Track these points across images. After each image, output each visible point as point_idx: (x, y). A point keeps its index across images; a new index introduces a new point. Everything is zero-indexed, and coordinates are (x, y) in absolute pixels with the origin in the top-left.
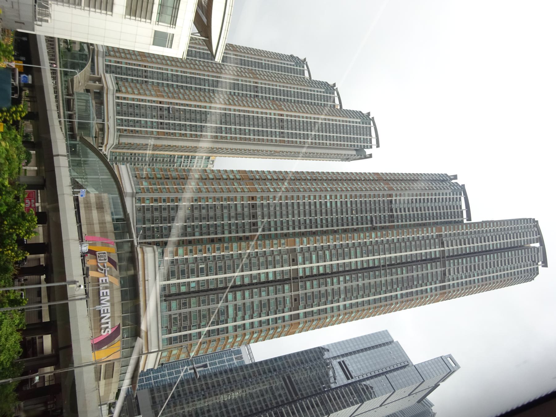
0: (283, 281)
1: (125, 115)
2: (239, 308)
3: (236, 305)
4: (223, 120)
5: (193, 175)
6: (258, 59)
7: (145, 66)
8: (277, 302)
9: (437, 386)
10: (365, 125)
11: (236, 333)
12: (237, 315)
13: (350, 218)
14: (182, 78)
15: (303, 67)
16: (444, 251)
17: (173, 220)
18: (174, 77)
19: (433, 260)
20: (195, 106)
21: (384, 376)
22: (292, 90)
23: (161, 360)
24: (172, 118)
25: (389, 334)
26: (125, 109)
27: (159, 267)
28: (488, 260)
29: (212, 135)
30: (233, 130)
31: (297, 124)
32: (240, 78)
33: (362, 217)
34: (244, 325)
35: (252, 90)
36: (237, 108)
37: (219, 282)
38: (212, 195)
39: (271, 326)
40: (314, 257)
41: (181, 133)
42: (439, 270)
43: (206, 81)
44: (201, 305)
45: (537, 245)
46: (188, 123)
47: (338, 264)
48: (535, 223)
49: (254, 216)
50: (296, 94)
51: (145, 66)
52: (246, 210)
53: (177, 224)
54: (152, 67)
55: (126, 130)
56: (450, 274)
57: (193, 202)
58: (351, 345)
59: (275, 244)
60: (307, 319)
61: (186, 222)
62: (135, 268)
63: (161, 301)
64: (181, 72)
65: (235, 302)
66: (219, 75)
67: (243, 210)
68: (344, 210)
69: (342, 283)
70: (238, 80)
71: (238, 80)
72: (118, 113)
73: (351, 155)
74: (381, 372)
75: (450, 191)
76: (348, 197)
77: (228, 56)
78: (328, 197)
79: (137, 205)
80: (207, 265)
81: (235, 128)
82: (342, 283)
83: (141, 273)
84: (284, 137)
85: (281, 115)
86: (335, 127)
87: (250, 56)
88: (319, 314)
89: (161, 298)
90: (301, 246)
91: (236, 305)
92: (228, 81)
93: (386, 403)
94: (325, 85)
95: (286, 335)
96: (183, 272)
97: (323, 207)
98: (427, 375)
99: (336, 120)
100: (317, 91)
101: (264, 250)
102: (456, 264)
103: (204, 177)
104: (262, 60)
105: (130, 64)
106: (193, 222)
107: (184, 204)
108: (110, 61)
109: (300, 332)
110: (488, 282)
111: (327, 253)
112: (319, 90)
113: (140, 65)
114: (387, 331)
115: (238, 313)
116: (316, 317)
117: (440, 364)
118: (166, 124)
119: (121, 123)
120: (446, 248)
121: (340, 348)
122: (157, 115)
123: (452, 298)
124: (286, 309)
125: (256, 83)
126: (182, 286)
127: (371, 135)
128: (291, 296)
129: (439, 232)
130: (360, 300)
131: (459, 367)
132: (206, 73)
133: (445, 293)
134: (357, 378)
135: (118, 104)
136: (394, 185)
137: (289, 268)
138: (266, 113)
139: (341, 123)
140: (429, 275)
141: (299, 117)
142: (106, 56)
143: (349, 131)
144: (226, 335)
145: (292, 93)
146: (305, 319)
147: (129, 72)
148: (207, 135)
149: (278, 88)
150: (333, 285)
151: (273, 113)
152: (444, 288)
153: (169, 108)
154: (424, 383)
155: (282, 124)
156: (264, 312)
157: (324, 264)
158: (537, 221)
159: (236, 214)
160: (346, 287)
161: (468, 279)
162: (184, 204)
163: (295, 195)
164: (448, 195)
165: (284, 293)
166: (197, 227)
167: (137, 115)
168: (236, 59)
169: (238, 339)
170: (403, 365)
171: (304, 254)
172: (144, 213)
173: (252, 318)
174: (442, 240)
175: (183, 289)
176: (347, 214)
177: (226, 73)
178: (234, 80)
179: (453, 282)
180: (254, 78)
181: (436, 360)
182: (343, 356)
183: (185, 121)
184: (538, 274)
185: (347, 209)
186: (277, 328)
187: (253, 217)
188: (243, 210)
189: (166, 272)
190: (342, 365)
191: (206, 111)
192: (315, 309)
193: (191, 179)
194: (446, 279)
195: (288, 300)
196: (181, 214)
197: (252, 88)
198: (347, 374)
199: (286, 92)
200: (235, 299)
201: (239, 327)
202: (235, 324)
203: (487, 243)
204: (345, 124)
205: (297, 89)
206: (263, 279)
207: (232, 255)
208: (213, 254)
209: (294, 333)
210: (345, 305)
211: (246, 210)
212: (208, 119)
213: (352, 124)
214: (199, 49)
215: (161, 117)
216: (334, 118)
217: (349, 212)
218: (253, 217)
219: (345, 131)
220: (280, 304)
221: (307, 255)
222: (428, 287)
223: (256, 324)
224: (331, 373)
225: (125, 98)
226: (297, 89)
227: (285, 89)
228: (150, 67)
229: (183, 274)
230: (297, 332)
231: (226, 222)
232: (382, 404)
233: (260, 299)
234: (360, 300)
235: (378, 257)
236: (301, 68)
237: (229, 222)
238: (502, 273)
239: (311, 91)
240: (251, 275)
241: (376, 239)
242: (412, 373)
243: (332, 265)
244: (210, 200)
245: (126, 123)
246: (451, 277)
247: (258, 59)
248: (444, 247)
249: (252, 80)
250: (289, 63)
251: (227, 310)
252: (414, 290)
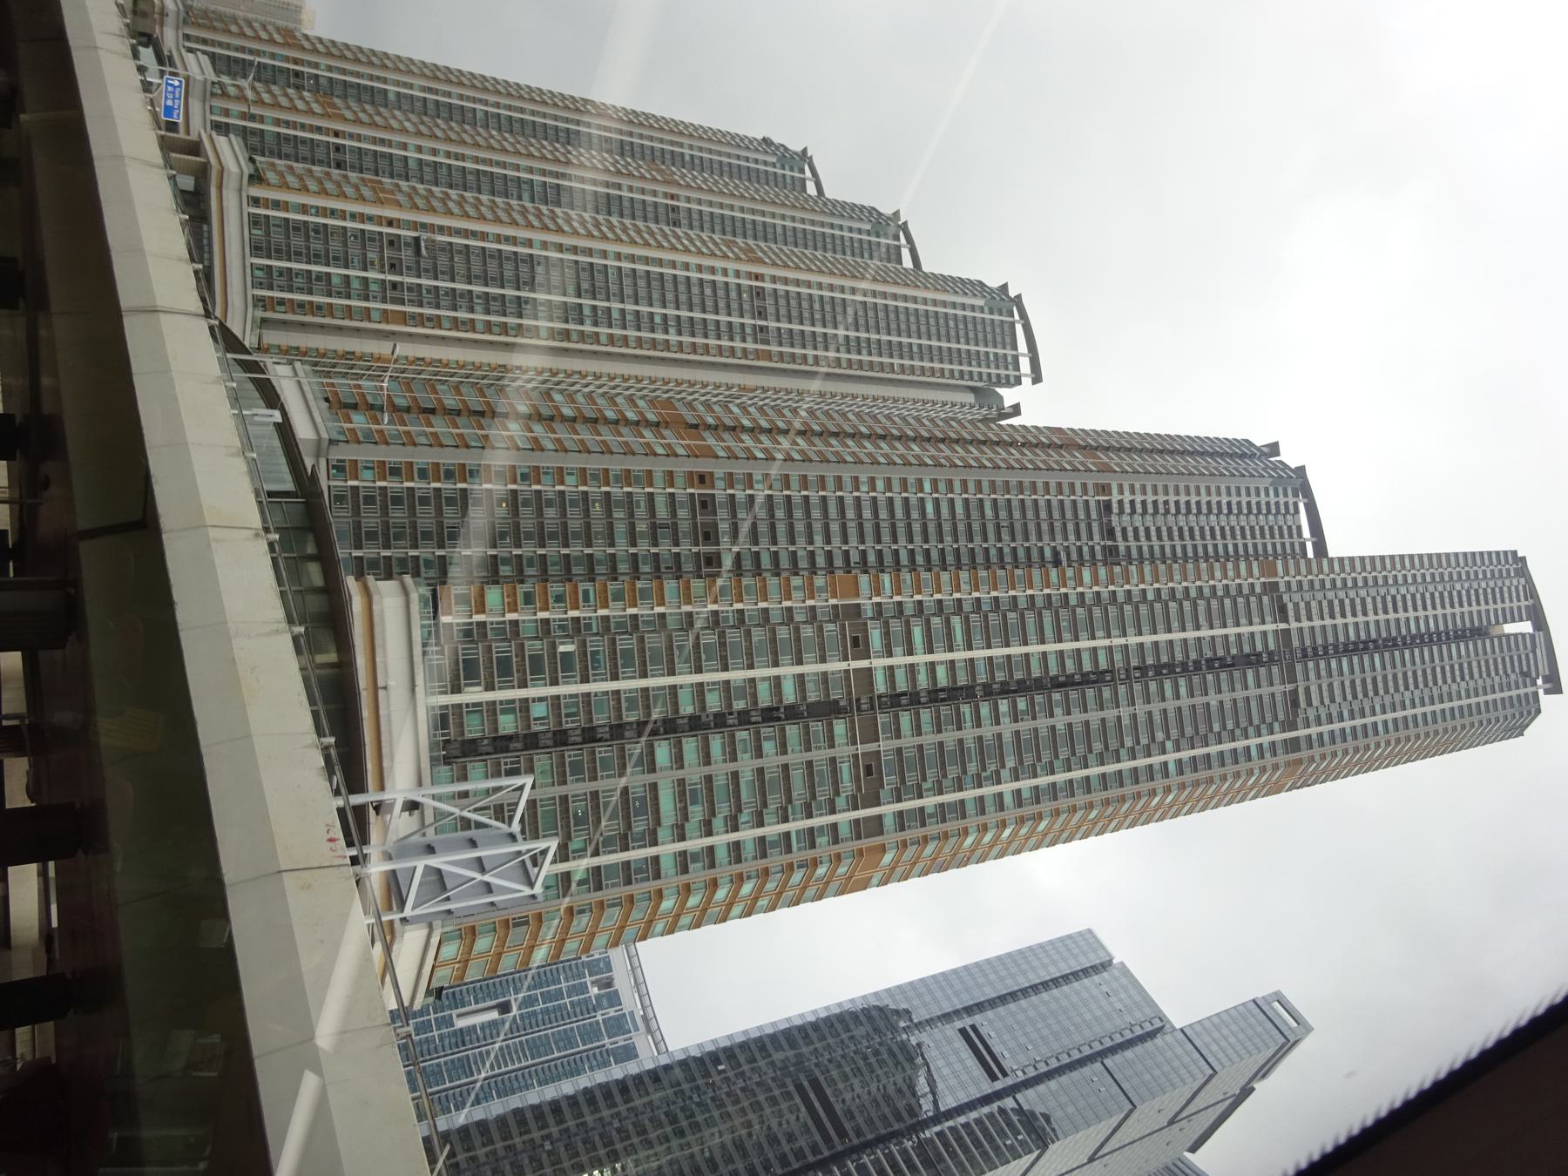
0: (829, 710)
1: (280, 254)
2: (694, 792)
3: (681, 782)
4: (585, 286)
5: (511, 405)
6: (672, 143)
7: (336, 134)
8: (811, 774)
9: (1247, 1091)
10: (996, 317)
11: (684, 878)
12: (686, 818)
13: (993, 552)
14: (450, 174)
15: (802, 171)
16: (1287, 633)
17: (454, 536)
18: (426, 169)
19: (1252, 660)
20: (498, 239)
21: (1098, 1065)
22: (778, 222)
23: (439, 973)
24: (426, 270)
25: (1098, 941)
26: (277, 237)
27: (424, 645)
28: (1408, 664)
29: (552, 329)
30: (615, 315)
31: (805, 304)
32: (625, 182)
33: (1028, 549)
34: (711, 849)
35: (662, 217)
36: (626, 250)
37: (624, 705)
38: (573, 462)
39: (797, 855)
40: (917, 633)
41: (456, 319)
42: (1278, 689)
43: (524, 186)
44: (569, 778)
45: (1526, 627)
46: (477, 289)
47: (990, 658)
48: (1515, 564)
49: (710, 535)
50: (789, 233)
51: (336, 134)
52: (683, 513)
53: (466, 552)
54: (359, 138)
55: (281, 302)
56: (1309, 704)
57: (515, 482)
58: (992, 977)
59: (796, 588)
60: (908, 835)
61: (494, 546)
62: (344, 644)
63: (433, 759)
64: (448, 155)
65: (680, 774)
66: (561, 170)
67: (674, 514)
68: (976, 526)
69: (1005, 720)
70: (619, 187)
71: (619, 187)
72: (257, 249)
73: (963, 406)
74: (1087, 1051)
75: (1266, 482)
76: (985, 486)
77: (581, 129)
78: (927, 487)
79: (333, 483)
80: (583, 644)
81: (623, 311)
82: (1007, 720)
83: (361, 661)
84: (768, 343)
85: (757, 277)
86: (912, 319)
87: (645, 132)
88: (944, 821)
89: (431, 750)
90: (876, 599)
91: (681, 782)
92: (589, 187)
93: (1106, 1150)
94: (870, 213)
95: (842, 893)
96: (505, 667)
97: (915, 515)
98: (1221, 1055)
99: (915, 300)
100: (851, 230)
101: (762, 605)
102: (1323, 673)
103: (545, 412)
104: (681, 145)
105: (287, 124)
106: (519, 546)
107: (486, 486)
108: (226, 113)
109: (884, 882)
110: (1412, 731)
111: (956, 621)
112: (856, 225)
113: (319, 130)
114: (1090, 931)
115: (691, 808)
116: (933, 829)
117: (1253, 1021)
118: (410, 289)
119: (268, 278)
120: (1294, 625)
121: (958, 987)
122: (382, 259)
123: (1313, 784)
124: (841, 802)
125: (672, 197)
126: (504, 712)
127: (1015, 347)
128: (856, 756)
129: (1269, 576)
130: (1060, 777)
131: (1309, 1029)
132: (523, 162)
133: (1299, 762)
134: (1019, 1073)
135: (255, 221)
136: (1113, 460)
137: (843, 666)
138: (713, 270)
139: (931, 308)
140: (1253, 704)
141: (809, 284)
142: (213, 94)
143: (952, 333)
144: (653, 885)
145: (779, 230)
146: (901, 836)
147: (286, 149)
148: (537, 327)
149: (738, 214)
150: (979, 725)
151: (731, 270)
152: (1293, 745)
153: (417, 239)
154: (1217, 1077)
155: (761, 303)
156: (772, 807)
157: (949, 656)
158: (1523, 559)
159: (654, 527)
160: (1017, 733)
161: (1358, 722)
162: (486, 486)
163: (830, 473)
164: (1262, 494)
165: (832, 746)
166: (531, 563)
167: (315, 258)
168: (608, 140)
169: (693, 901)
170: (1148, 1028)
171: (886, 624)
172: (356, 511)
173: (735, 829)
174: (1280, 598)
175: (507, 724)
176: (986, 540)
177: (582, 165)
178: (607, 185)
179: (1320, 729)
180: (667, 182)
181: (1242, 1009)
182: (969, 1010)
183: (470, 283)
184: (1538, 711)
185: (984, 526)
186: (815, 863)
187: (707, 536)
188: (674, 514)
189: (446, 662)
190: (974, 1041)
191: (531, 256)
192: (930, 802)
193: (506, 415)
194: (1299, 720)
195: (845, 770)
196: (478, 518)
197: (661, 210)
198: (990, 1064)
199: (760, 228)
200: (678, 760)
201: (696, 857)
202: (681, 846)
203: (1402, 615)
204: (941, 310)
205: (793, 219)
206: (765, 698)
207: (662, 616)
208: (602, 612)
209: (864, 885)
210: (1019, 792)
211: (683, 513)
212: (539, 279)
213: (960, 312)
214: (498, 105)
215: (394, 267)
216: (910, 292)
217: (991, 535)
218: (707, 536)
219: (943, 331)
220: (822, 784)
221: (896, 626)
222: (1253, 742)
223: (749, 850)
224: (922, 1085)
225: (277, 205)
226: (793, 219)
227: (759, 218)
228: (351, 136)
229: (504, 671)
230: (875, 881)
231: (622, 547)
232: (1096, 1152)
233: (759, 763)
234: (1060, 777)
235: (1106, 642)
236: (797, 175)
237: (633, 550)
238: (1438, 707)
239: (832, 226)
240: (727, 682)
241: (1096, 589)
242: (1179, 1051)
243: (972, 660)
244: (570, 480)
245: (283, 282)
246: (1311, 713)
247: (672, 143)
248: (1287, 621)
249: (661, 189)
250: (761, 157)
251: (656, 798)
252: (1213, 749)
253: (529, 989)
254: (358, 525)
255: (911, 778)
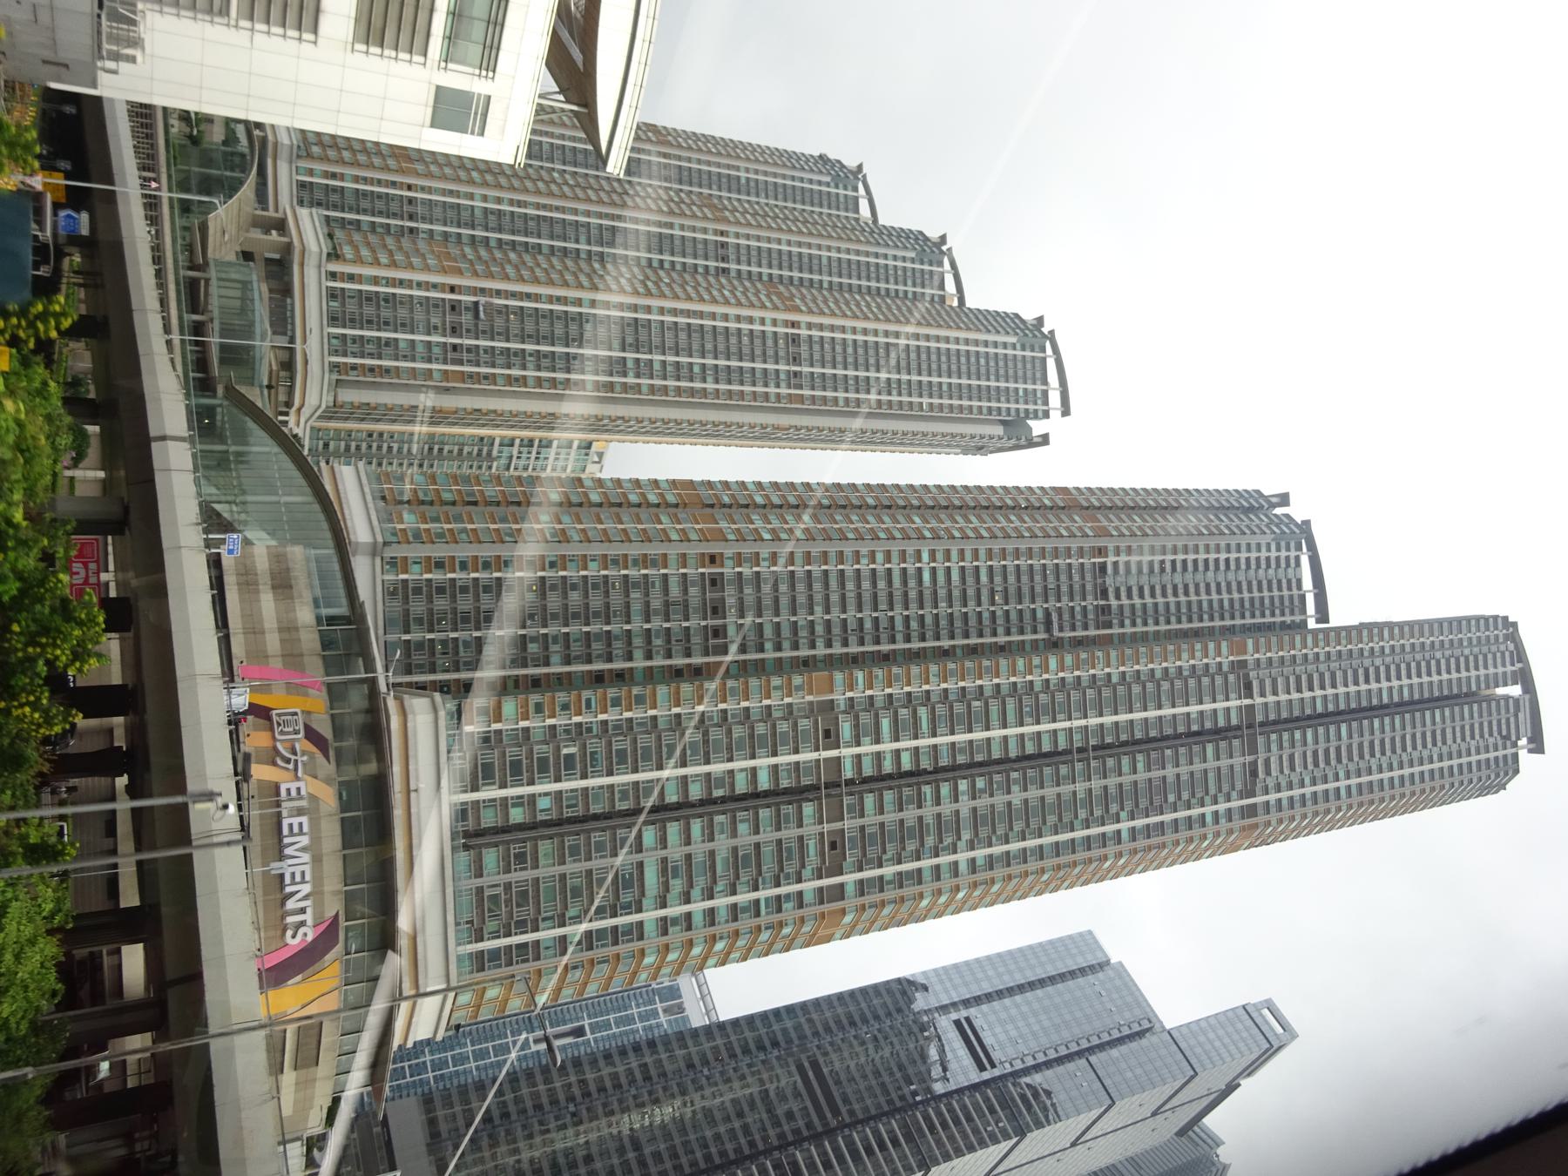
0: (798, 793)
1: (353, 323)
2: (675, 869)
3: (664, 860)
4: (630, 340)
5: (545, 493)
6: (729, 167)
7: (409, 188)
8: (780, 851)
9: (1231, 1087)
10: (1028, 353)
11: (664, 939)
12: (667, 890)
13: (986, 615)
14: (513, 221)
15: (856, 189)
16: (1251, 708)
17: (488, 619)
18: (491, 217)
19: (1220, 733)
20: (550, 299)
21: (1083, 1062)
22: (824, 253)
23: (455, 1015)
24: (484, 332)
25: (1096, 942)
26: (352, 306)
27: (449, 752)
28: (1377, 733)
29: (597, 382)
30: (657, 366)
31: (839, 349)
32: (677, 221)
33: (1021, 611)
34: (689, 915)
35: (711, 254)
36: (668, 304)
37: (617, 796)
39: (764, 919)
40: (885, 724)
41: (509, 376)
42: (1238, 761)
43: (582, 230)
44: (568, 859)
45: (1515, 690)
46: (530, 347)
47: (953, 744)
48: (1509, 629)
49: (717, 610)
50: (834, 264)
51: (409, 188)
52: (694, 591)
53: (499, 633)
54: (430, 190)
55: (354, 367)
56: (1268, 773)
57: (543, 569)
58: (991, 973)
59: (776, 688)
60: (867, 899)
61: (524, 627)
62: (382, 754)
63: (454, 849)
64: (511, 202)
65: (663, 853)
66: (617, 212)
67: (685, 591)
68: (971, 592)
69: (963, 798)
70: (671, 226)
71: (671, 226)
72: (334, 320)
73: (991, 438)
74: (1074, 1048)
75: (1269, 538)
76: (982, 554)
77: (642, 157)
78: (925, 556)
79: (387, 577)
80: (584, 746)
81: (664, 362)
82: (965, 798)
83: (397, 769)
84: (801, 387)
85: (794, 324)
86: (944, 359)
87: (704, 157)
88: (901, 886)
89: (453, 839)
90: (850, 694)
91: (664, 860)
92: (642, 228)
93: (1088, 1136)
94: (917, 239)
95: (808, 945)
96: (516, 768)
97: (912, 583)
98: (1204, 1057)
99: (947, 340)
100: (895, 258)
101: (744, 704)
102: (1286, 744)
103: (574, 499)
104: (738, 168)
105: (365, 180)
106: (545, 626)
107: (518, 574)
108: (311, 172)
109: (846, 936)
110: (1377, 795)
111: (923, 712)
112: (900, 253)
113: (394, 184)
114: (1090, 932)
115: (671, 882)
116: (890, 894)
117: (1240, 1026)
118: (469, 350)
119: (341, 345)
120: (1259, 700)
121: (957, 981)
122: (444, 323)
123: (1273, 842)
124: (807, 873)
125: (722, 233)
126: (514, 805)
127: (1045, 382)
128: (822, 834)
129: (1238, 654)
130: (1014, 846)
131: (1294, 1036)
132: (582, 207)
133: (1256, 826)
134: (1007, 1065)
135: (333, 294)
136: (1112, 523)
137: (814, 756)
138: (751, 320)
139: (963, 347)
140: (1211, 775)
141: (843, 329)
142: (299, 157)
143: (983, 370)
144: (637, 945)
145: (825, 261)
146: (861, 900)
148: (583, 381)
149: (784, 248)
150: (938, 804)
151: (769, 319)
152: (1251, 811)
153: (476, 304)
154: (1197, 1080)
155: (796, 350)
156: (743, 879)
157: (914, 743)
158: (1515, 625)
159: (667, 604)
160: (975, 810)
161: (1320, 788)
162: (518, 574)
163: (832, 549)
164: (1264, 549)
165: (800, 825)
166: (555, 640)
167: (385, 324)
169: (672, 957)
170: (1136, 1028)
171: (857, 717)
172: (406, 599)
173: (711, 897)
174: (1247, 676)
175: (517, 815)
176: (979, 604)
177: (637, 207)
178: (660, 224)
179: (1279, 795)
180: (717, 220)
181: (1230, 1014)
182: (966, 1003)
183: (523, 342)
184: (1517, 771)
185: (978, 591)
186: (781, 925)
187: (715, 611)
188: (685, 591)
190: (966, 1030)
191: (580, 314)
192: (889, 871)
193: (539, 504)
194: (1259, 786)
195: (812, 846)
196: (511, 603)
197: (711, 247)
198: (980, 1055)
199: (806, 260)
200: (663, 842)
201: (675, 921)
202: (662, 913)
203: (1374, 686)
204: (972, 348)
205: (839, 250)
206: (741, 786)
207: (654, 718)
208: (602, 717)
209: (828, 939)
210: (973, 860)
211: (694, 591)
212: (587, 335)
213: (991, 350)
214: (563, 137)
215: (455, 331)
216: (943, 333)
217: (985, 598)
218: (715, 611)
219: (973, 369)
220: (789, 858)
221: (865, 718)
222: (1208, 810)
223: (722, 915)
224: (933, 1053)
225: (352, 278)
226: (839, 250)
227: (805, 251)
228: (423, 189)
229: (516, 772)
230: (838, 935)
231: (637, 625)
232: (1078, 1138)
233: (733, 842)
234: (1014, 846)
235: (1067, 724)
236: (850, 193)
237: (647, 626)
238: (1417, 769)
239: (877, 255)
240: (709, 774)
241: (1061, 675)
242: (1163, 1052)
243: (935, 746)
244: (593, 565)
245: (355, 348)
246: (1271, 782)
247: (729, 167)
248: (1251, 697)
249: (711, 226)
250: (815, 177)
251: (642, 873)
252: (1168, 817)
253: (720, 663)
254: (407, 613)
255: (872, 852)
